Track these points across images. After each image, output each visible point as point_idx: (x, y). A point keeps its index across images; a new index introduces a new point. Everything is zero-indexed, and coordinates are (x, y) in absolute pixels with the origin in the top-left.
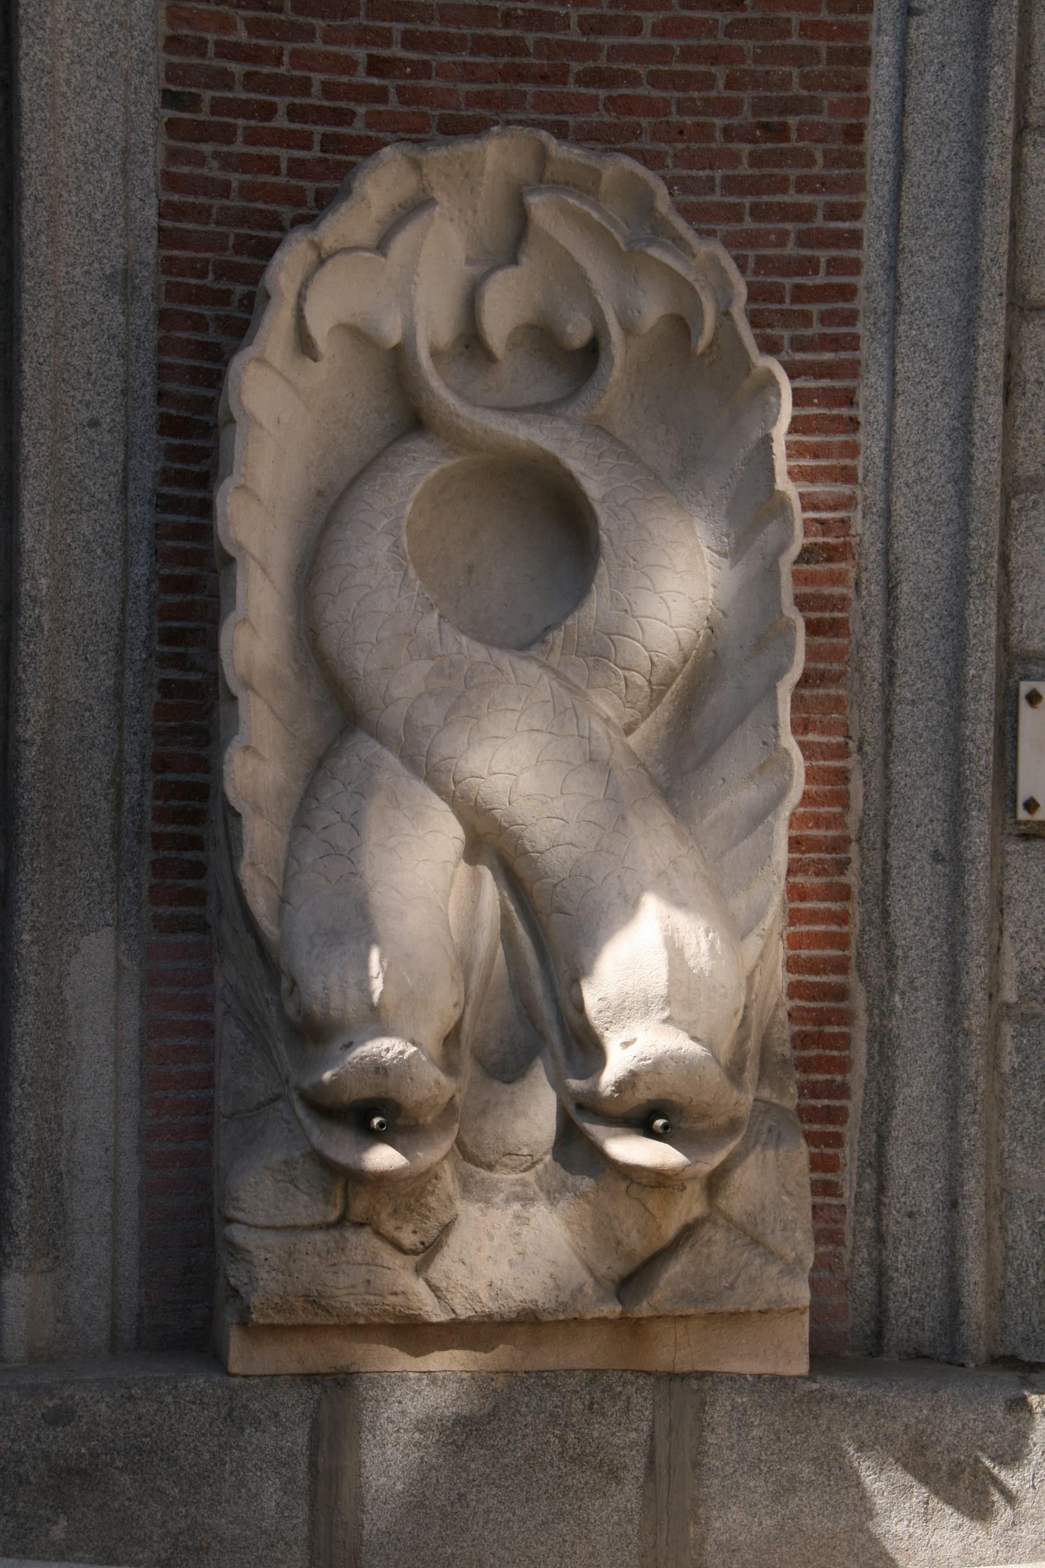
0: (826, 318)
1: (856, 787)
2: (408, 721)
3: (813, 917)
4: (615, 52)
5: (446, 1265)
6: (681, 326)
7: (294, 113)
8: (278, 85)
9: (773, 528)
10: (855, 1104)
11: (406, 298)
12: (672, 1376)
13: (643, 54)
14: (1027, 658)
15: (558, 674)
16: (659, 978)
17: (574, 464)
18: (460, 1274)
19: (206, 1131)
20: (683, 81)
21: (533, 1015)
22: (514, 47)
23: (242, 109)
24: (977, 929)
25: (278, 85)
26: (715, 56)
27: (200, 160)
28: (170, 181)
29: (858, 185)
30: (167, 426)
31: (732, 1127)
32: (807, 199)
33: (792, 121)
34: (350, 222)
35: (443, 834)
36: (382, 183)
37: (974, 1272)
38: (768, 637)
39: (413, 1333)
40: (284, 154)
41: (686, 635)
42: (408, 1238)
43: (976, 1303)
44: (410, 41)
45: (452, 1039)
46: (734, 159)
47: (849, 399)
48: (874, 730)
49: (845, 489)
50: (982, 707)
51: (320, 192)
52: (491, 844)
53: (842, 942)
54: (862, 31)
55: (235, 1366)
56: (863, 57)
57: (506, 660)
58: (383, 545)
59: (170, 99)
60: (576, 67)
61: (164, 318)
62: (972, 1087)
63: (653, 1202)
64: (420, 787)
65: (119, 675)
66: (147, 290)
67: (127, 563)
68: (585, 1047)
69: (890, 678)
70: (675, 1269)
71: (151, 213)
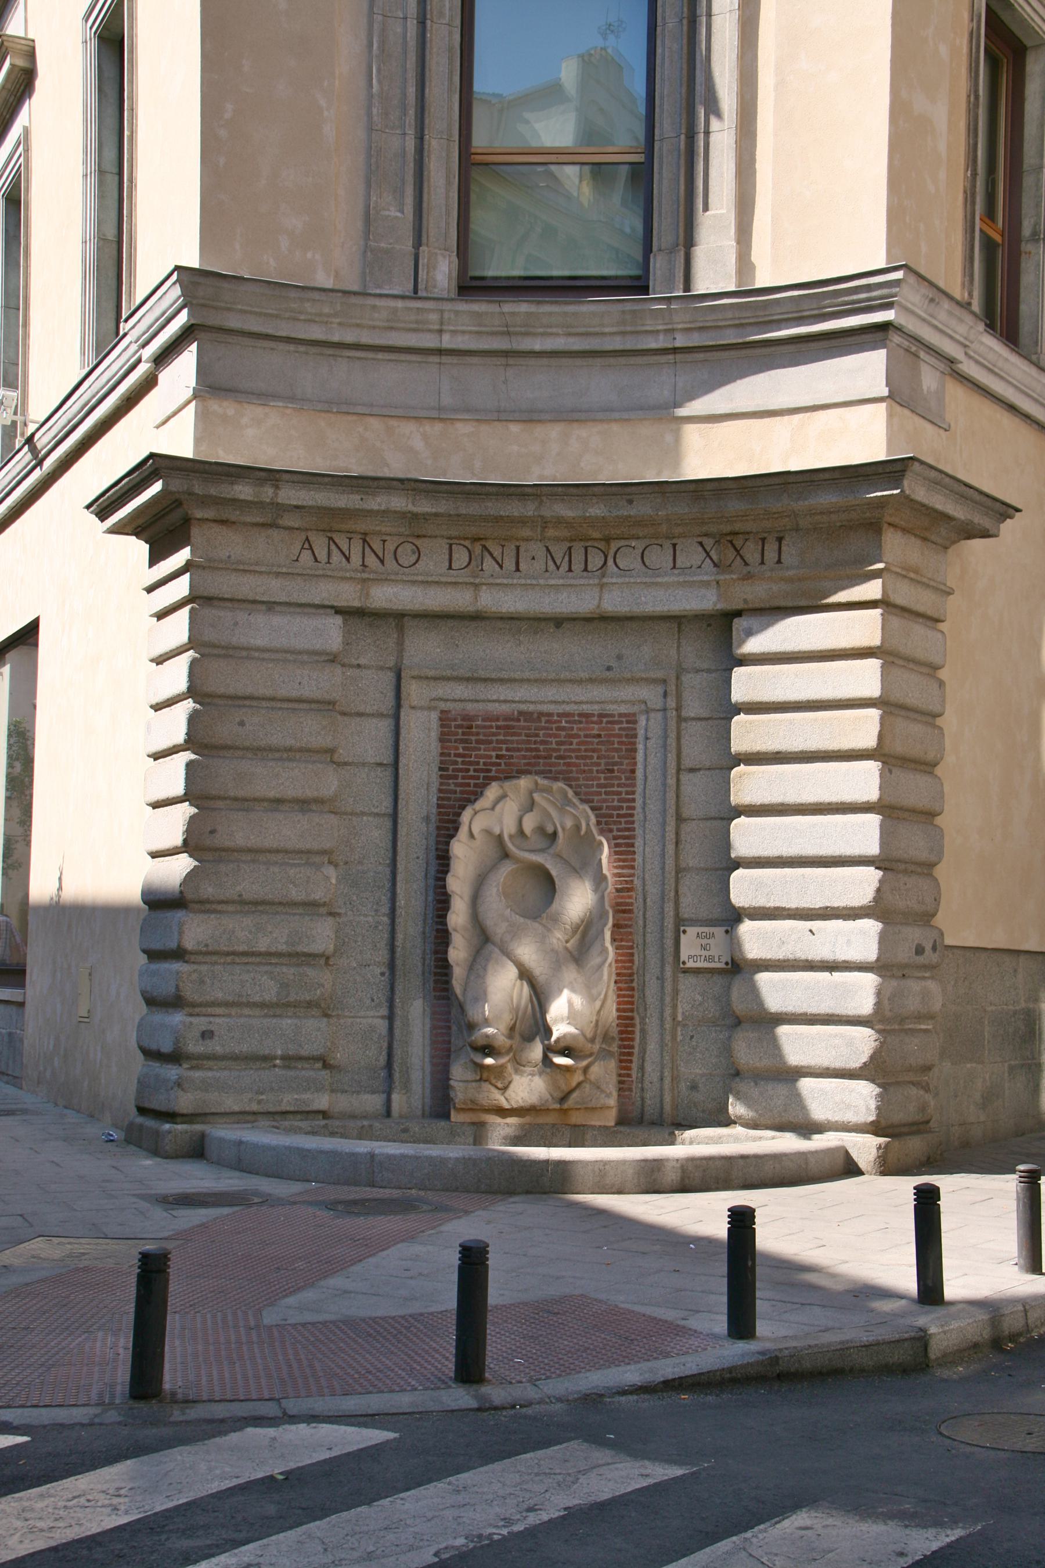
0: (626, 823)
1: (636, 958)
2: (501, 940)
3: (624, 996)
4: (565, 750)
5: (510, 1092)
6: (577, 827)
7: (475, 770)
8: (470, 763)
9: (604, 884)
10: (636, 1051)
11: (501, 822)
12: (575, 1126)
13: (574, 750)
14: (684, 920)
15: (544, 926)
16: (566, 1012)
17: (548, 866)
18: (513, 1095)
19: (449, 1057)
20: (586, 757)
21: (533, 1025)
22: (537, 750)
23: (461, 770)
24: (668, 999)
25: (470, 763)
26: (594, 751)
27: (449, 785)
28: (440, 791)
29: (634, 785)
30: (438, 857)
31: (591, 1055)
32: (620, 789)
33: (616, 768)
34: (482, 803)
35: (512, 972)
36: (492, 792)
37: (667, 1098)
39: (502, 1112)
40: (472, 782)
41: (581, 914)
42: (500, 1085)
43: (668, 1108)
44: (508, 750)
45: (512, 1029)
46: (599, 779)
47: (633, 845)
48: (641, 941)
49: (632, 871)
50: (669, 934)
51: (472, 796)
52: (525, 974)
53: (632, 1003)
54: (634, 743)
55: (453, 1119)
56: (635, 750)
57: (529, 922)
58: (495, 890)
59: (441, 769)
60: (554, 754)
61: (438, 828)
62: (667, 1045)
63: (568, 1075)
64: (505, 958)
65: (424, 927)
66: (433, 820)
67: (427, 895)
68: (548, 1032)
69: (645, 926)
70: (575, 1095)
71: (435, 800)
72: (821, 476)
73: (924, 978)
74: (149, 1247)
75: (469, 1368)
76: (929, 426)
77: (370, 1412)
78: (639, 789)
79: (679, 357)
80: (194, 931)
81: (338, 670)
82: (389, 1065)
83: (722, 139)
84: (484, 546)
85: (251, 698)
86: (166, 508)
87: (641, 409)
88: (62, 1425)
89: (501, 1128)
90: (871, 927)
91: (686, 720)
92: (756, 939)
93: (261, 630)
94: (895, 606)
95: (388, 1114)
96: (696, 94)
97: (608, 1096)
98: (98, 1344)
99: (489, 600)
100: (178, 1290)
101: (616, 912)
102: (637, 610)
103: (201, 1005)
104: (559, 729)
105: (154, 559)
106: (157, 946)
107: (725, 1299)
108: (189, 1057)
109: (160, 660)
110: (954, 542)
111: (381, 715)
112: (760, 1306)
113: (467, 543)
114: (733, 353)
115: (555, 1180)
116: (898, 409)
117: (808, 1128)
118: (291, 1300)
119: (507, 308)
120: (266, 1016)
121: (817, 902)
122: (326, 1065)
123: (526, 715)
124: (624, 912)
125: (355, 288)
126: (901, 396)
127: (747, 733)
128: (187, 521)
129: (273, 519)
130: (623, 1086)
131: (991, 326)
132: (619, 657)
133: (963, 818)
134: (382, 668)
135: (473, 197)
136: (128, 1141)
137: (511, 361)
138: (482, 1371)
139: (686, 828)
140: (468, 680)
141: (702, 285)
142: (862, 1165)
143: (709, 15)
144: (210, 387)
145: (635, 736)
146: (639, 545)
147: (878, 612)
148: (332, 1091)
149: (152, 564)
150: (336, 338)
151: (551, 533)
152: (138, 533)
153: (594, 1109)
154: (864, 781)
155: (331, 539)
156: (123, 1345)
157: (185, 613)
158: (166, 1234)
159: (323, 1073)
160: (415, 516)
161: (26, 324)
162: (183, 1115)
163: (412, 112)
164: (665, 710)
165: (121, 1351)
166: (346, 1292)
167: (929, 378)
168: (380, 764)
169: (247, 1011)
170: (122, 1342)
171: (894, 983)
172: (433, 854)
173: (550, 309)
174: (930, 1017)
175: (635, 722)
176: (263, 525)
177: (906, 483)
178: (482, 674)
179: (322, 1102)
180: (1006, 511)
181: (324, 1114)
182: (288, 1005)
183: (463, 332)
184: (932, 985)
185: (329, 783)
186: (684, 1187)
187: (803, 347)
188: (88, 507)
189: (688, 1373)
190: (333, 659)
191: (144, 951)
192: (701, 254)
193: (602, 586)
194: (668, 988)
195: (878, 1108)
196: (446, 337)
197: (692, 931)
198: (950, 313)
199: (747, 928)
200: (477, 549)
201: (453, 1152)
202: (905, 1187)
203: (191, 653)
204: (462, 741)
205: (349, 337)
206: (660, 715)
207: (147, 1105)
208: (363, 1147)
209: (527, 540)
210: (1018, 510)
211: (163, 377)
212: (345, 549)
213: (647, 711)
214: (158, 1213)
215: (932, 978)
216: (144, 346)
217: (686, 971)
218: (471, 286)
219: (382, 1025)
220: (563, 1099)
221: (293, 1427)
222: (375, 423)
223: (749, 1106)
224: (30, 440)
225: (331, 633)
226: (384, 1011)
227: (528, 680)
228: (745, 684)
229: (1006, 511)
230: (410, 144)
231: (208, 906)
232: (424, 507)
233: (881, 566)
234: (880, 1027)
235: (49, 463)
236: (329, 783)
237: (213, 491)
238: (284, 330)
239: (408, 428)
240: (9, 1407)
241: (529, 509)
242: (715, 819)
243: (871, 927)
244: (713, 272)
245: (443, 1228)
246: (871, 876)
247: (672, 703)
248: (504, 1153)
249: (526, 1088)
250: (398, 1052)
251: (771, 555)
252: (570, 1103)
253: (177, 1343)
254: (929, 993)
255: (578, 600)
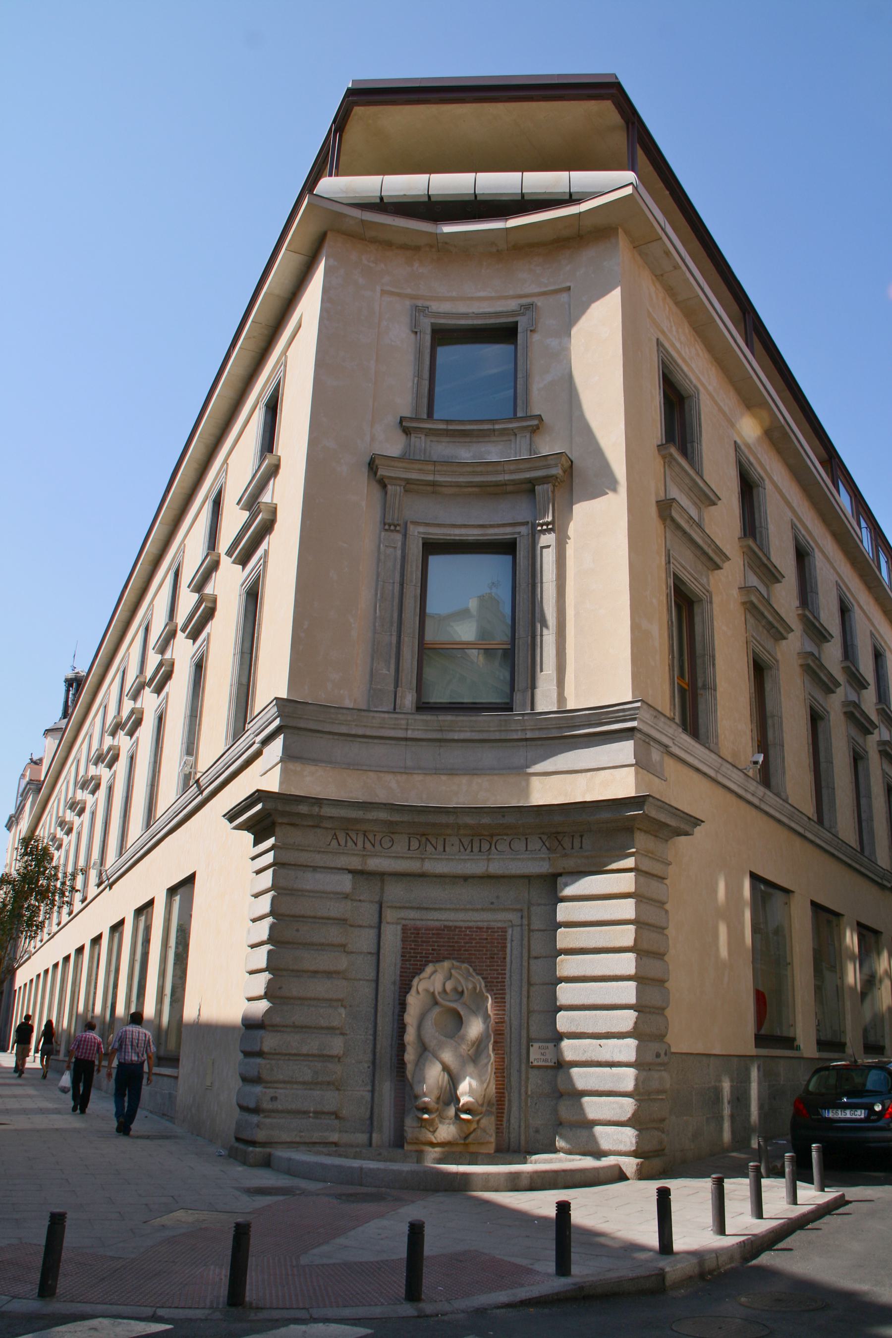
5: (437, 1134)
6: (475, 988)
8: (418, 953)
10: (506, 1111)
16: (468, 1089)
24: (523, 1083)
26: (484, 947)
28: (402, 968)
30: (400, 1004)
31: (481, 1113)
34: (425, 975)
36: (429, 969)
37: (523, 1137)
38: (488, 1036)
39: (433, 1145)
43: (523, 1142)
45: (438, 1098)
50: (524, 1047)
51: (419, 971)
52: (446, 1068)
56: (506, 947)
57: (448, 1040)
61: (400, 988)
68: (458, 1100)
70: (472, 1136)
72: (602, 804)
73: (660, 1071)
74: (240, 1220)
75: (413, 1292)
76: (656, 779)
77: (358, 1317)
78: (508, 968)
79: (528, 743)
80: (269, 1042)
81: (349, 903)
82: (371, 1118)
83: (549, 638)
84: (427, 839)
85: (303, 917)
86: (264, 818)
87: (509, 768)
88: (191, 1320)
89: (433, 1153)
90: (632, 1043)
91: (533, 931)
92: (570, 1049)
93: (310, 881)
94: (642, 871)
95: (370, 1145)
96: (536, 617)
97: (491, 1136)
98: (211, 1273)
99: (429, 867)
100: (255, 1242)
101: (495, 1035)
102: (507, 872)
103: (271, 1082)
104: (465, 935)
105: (256, 843)
106: (248, 1049)
107: (554, 1253)
108: (263, 1111)
109: (256, 896)
110: (671, 838)
111: (371, 927)
112: (574, 1257)
113: (418, 837)
114: (557, 741)
115: (462, 1183)
116: (640, 770)
117: (599, 1154)
118: (316, 1251)
119: (441, 718)
120: (306, 1089)
121: (603, 1030)
122: (337, 1117)
123: (448, 928)
124: (500, 1034)
125: (364, 708)
126: (641, 764)
127: (565, 938)
128: (274, 824)
129: (317, 823)
130: (499, 1130)
131: (685, 729)
132: (498, 897)
133: (680, 983)
134: (372, 902)
135: (425, 662)
136: (230, 1156)
137: (443, 744)
138: (420, 1294)
139: (533, 989)
140: (418, 908)
141: (540, 708)
142: (628, 1174)
143: (542, 583)
144: (288, 756)
145: (506, 939)
146: (508, 838)
147: (633, 874)
148: (340, 1131)
149: (255, 845)
150: (353, 732)
151: (462, 832)
152: (248, 830)
153: (482, 1144)
154: (627, 963)
155: (347, 834)
156: (224, 1274)
157: (270, 871)
158: (248, 1210)
159: (336, 1121)
160: (391, 823)
161: (200, 725)
162: (259, 1143)
163: (395, 625)
164: (521, 925)
165: (223, 1277)
166: (346, 1247)
167: (656, 755)
168: (370, 953)
169: (295, 1086)
170: (224, 1272)
171: (645, 1073)
172: (397, 1002)
173: (463, 719)
174: (664, 1091)
175: (506, 932)
176: (313, 826)
177: (646, 808)
178: (425, 905)
179: (335, 1137)
180: (697, 822)
181: (335, 1144)
182: (317, 1083)
183: (418, 730)
184: (664, 1074)
185: (343, 963)
186: (532, 1188)
187: (592, 738)
188: (224, 816)
189: (534, 1296)
190: (346, 897)
191: (242, 1052)
192: (539, 692)
193: (489, 860)
194: (523, 1077)
195: (637, 1142)
196: (409, 732)
197: (536, 1045)
198: (665, 723)
199: (566, 1043)
200: (423, 839)
201: (406, 1167)
202: (653, 1186)
203: (272, 892)
204: (413, 941)
205: (360, 732)
206: (519, 928)
207: (242, 1136)
208: (356, 1163)
209: (450, 835)
210: (703, 822)
211: (266, 751)
212: (354, 839)
213: (512, 926)
214: (245, 1198)
215: (665, 1070)
216: (257, 736)
217: (533, 1067)
218: (423, 707)
219: (368, 1096)
220: (466, 1138)
221: (316, 1325)
222: (371, 774)
223: (567, 1141)
224: (197, 782)
225: (345, 883)
226: (369, 1088)
227: (449, 909)
228: (564, 911)
229: (697, 822)
230: (394, 640)
231: (276, 1028)
232: (397, 818)
233: (634, 850)
234: (637, 1097)
235: (206, 793)
236: (343, 963)
237: (288, 809)
238: (328, 728)
239: (389, 777)
240: (163, 1307)
241: (451, 819)
242: (548, 984)
243: (632, 1043)
244: (545, 701)
245: (399, 1211)
246: (632, 1015)
247: (525, 922)
248: (433, 1168)
249: (446, 1131)
250: (376, 1110)
251: (577, 844)
252: (469, 1140)
253: (253, 1274)
254: (665, 1079)
255: (475, 867)
